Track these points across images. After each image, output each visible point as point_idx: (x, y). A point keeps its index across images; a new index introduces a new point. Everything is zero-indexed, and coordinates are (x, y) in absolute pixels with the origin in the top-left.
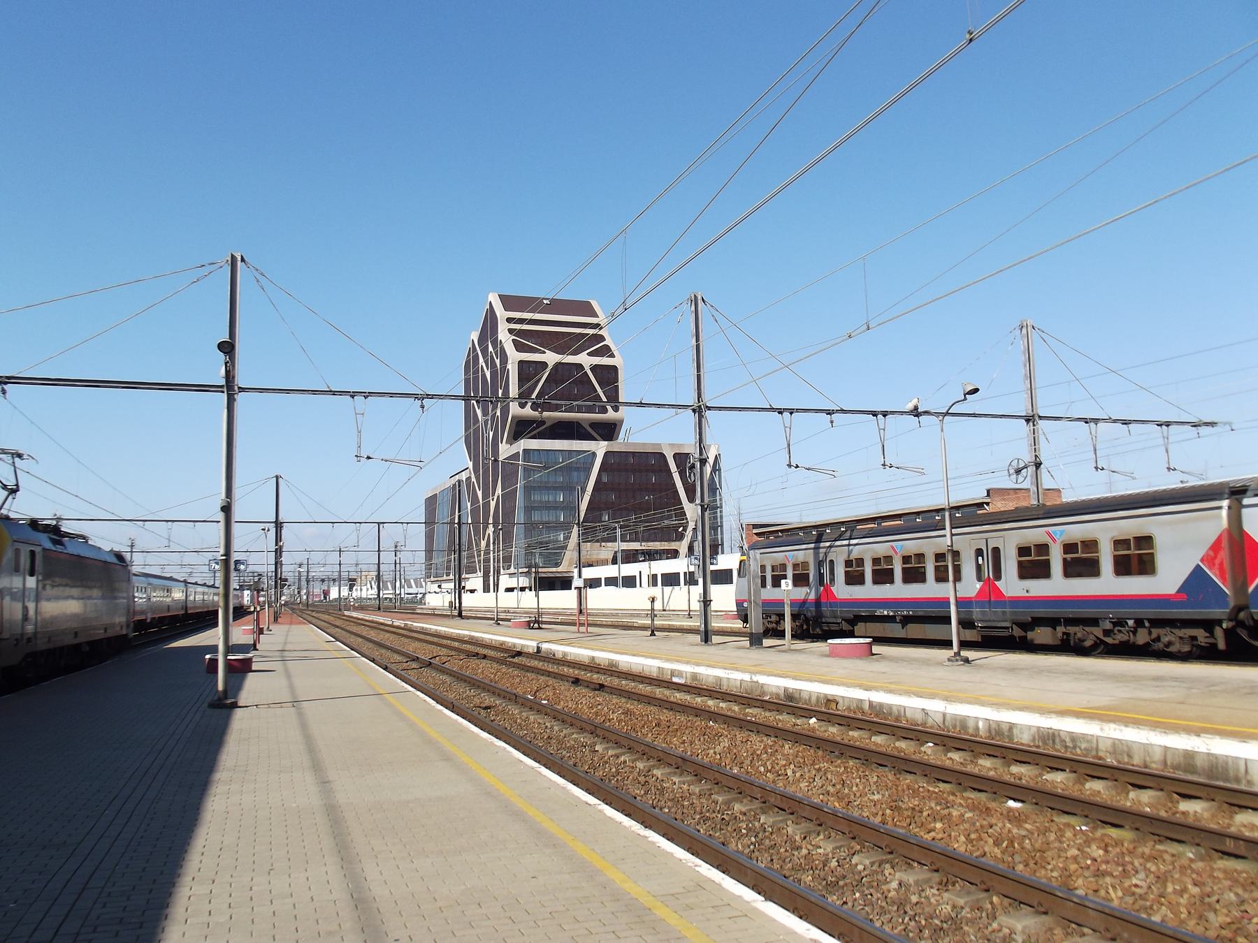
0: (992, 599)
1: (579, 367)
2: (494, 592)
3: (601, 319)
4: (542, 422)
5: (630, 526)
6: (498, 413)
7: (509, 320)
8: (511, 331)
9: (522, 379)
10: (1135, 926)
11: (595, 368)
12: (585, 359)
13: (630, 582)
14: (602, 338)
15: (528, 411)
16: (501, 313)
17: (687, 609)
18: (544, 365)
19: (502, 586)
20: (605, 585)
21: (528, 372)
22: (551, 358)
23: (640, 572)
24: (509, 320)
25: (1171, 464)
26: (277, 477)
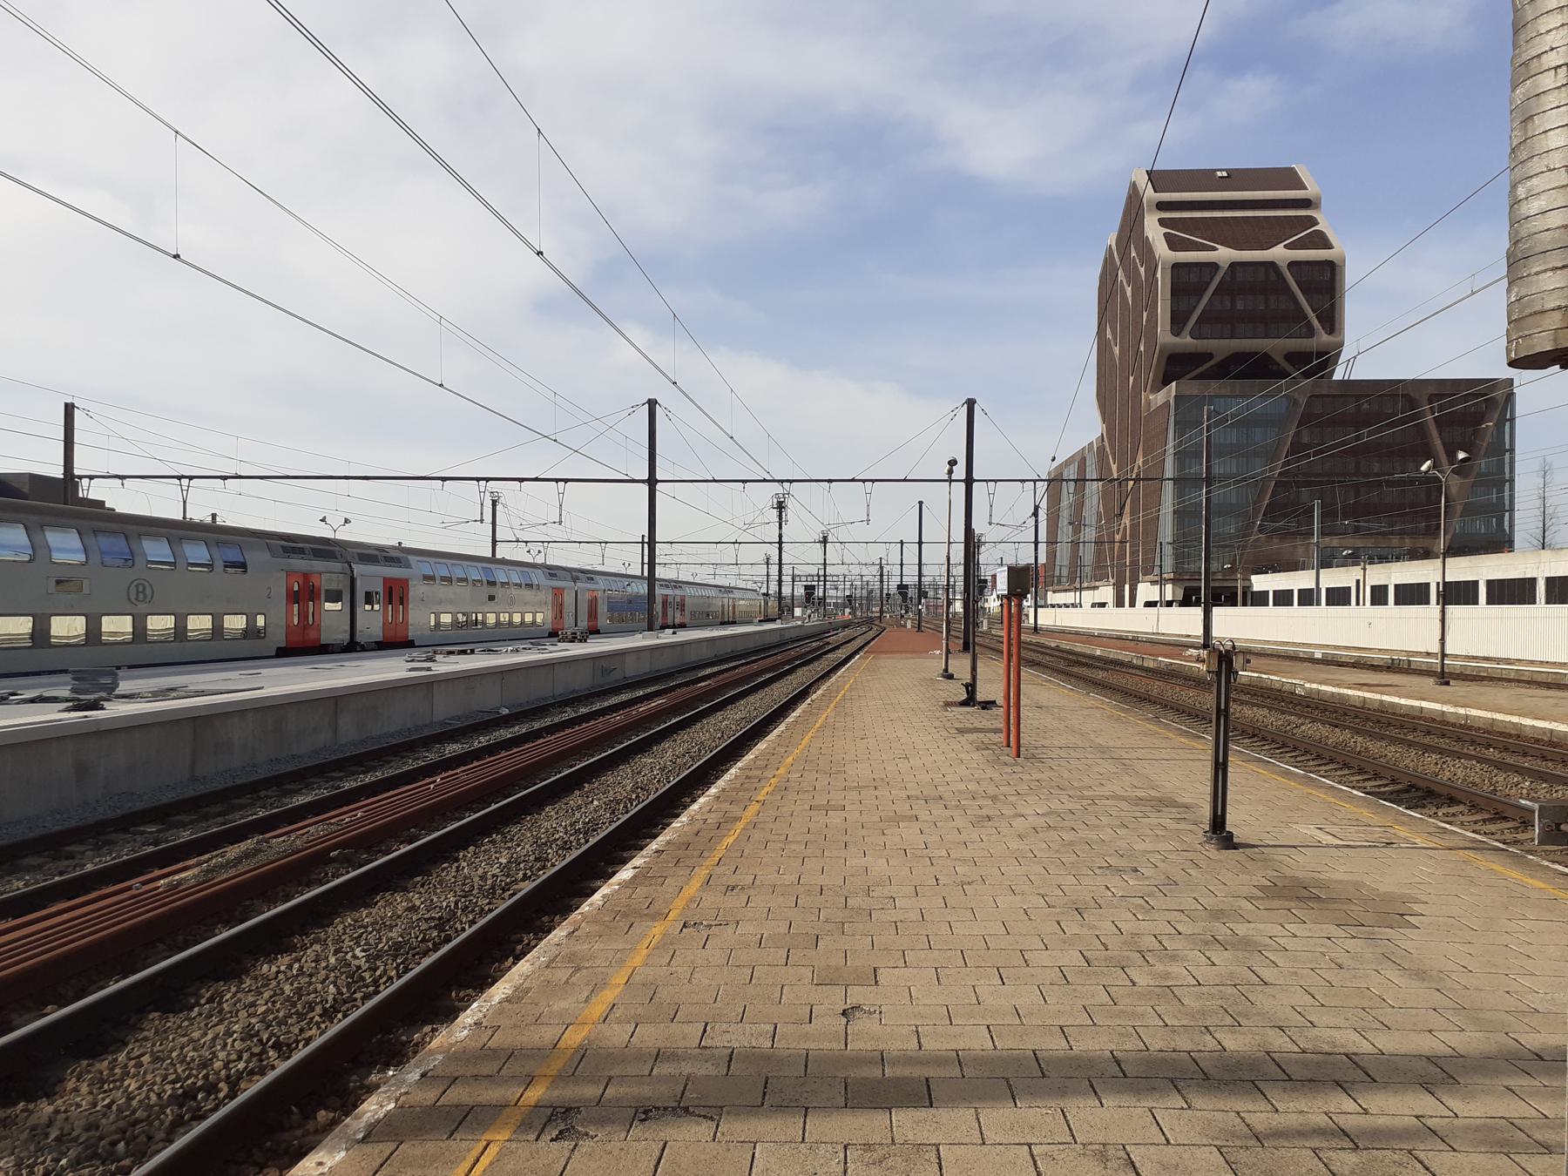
0: (1220, 577)
1: (1271, 266)
2: (1438, 604)
3: (1312, 189)
4: (1209, 356)
5: (1372, 529)
6: (1142, 348)
7: (1162, 206)
8: (1162, 222)
9: (1177, 291)
10: (1446, 570)
11: (1293, 265)
12: (1279, 253)
13: (1339, 597)
14: (1313, 222)
15: (1186, 341)
16: (1149, 194)
17: (1436, 648)
18: (1213, 267)
19: (1140, 600)
20: (1396, 603)
21: (1187, 281)
22: (1224, 254)
23: (69, 409)
24: (1162, 206)
25: (1438, 615)
26: (652, 404)
